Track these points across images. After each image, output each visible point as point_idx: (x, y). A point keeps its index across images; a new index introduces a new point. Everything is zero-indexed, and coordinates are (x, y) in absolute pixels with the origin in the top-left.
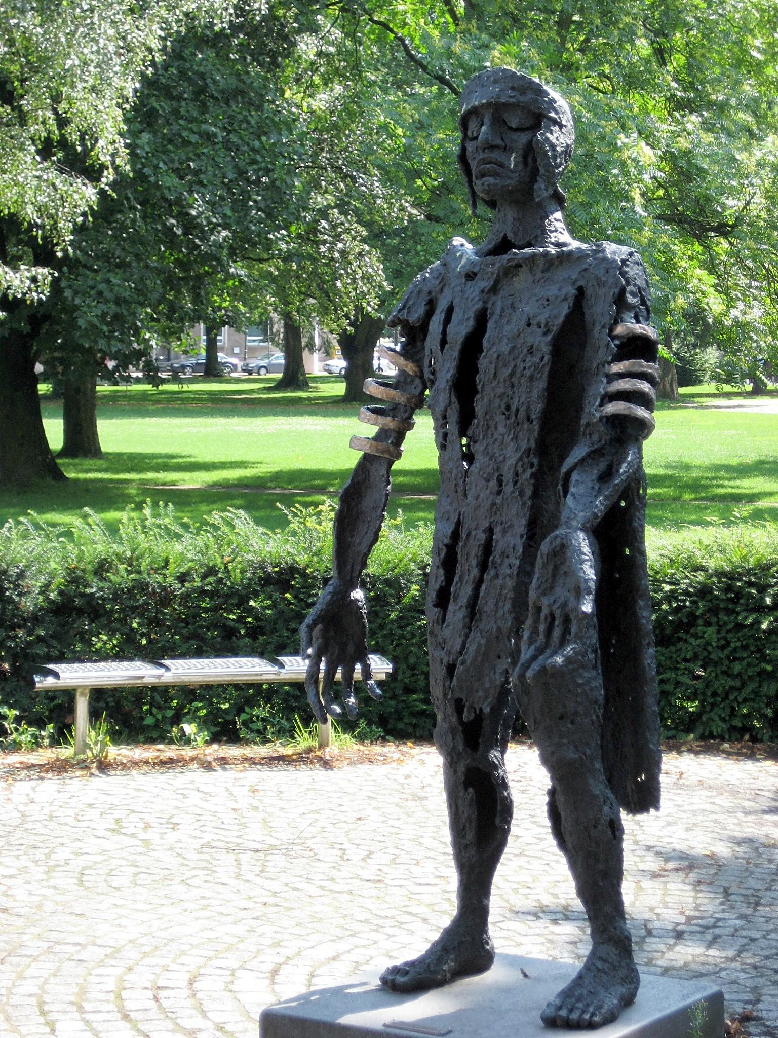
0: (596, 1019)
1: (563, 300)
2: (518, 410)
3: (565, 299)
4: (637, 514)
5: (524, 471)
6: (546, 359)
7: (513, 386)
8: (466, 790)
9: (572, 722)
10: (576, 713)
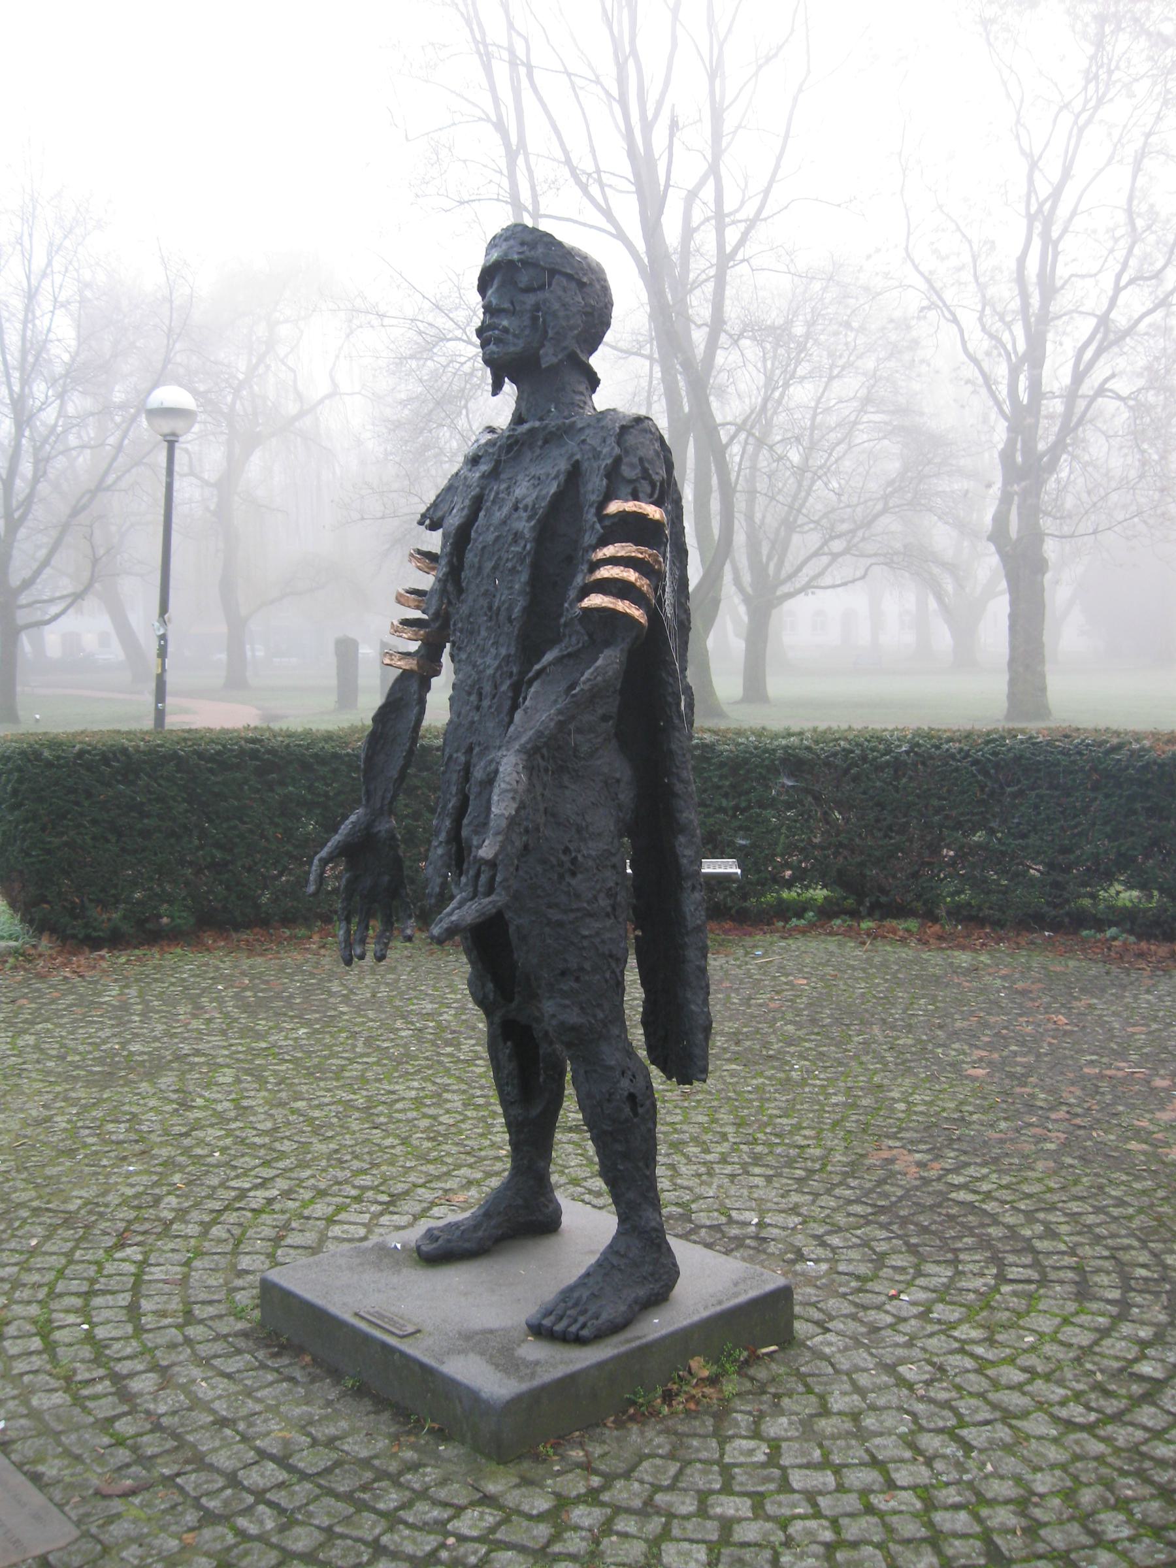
0: (585, 1333)
2: (499, 609)
3: (556, 477)
9: (577, 979)
10: (582, 969)
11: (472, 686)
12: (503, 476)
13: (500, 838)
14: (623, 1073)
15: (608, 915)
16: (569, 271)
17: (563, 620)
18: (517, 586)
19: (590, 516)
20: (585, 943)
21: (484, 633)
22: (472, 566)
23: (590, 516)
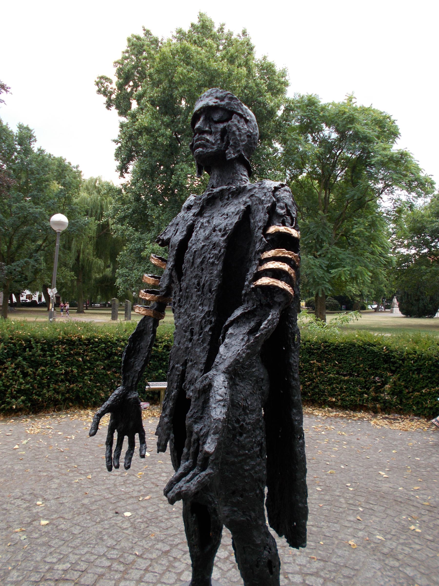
1: (236, 214)
2: (204, 285)
4: (293, 355)
5: (205, 326)
6: (222, 250)
7: (202, 270)
8: (192, 515)
9: (242, 496)
11: (187, 327)
12: (205, 215)
13: (217, 436)
14: (265, 548)
15: (258, 457)
16: (240, 112)
17: (244, 292)
18: (215, 272)
19: (259, 234)
20: (246, 474)
21: (194, 298)
22: (188, 261)
23: (259, 234)
